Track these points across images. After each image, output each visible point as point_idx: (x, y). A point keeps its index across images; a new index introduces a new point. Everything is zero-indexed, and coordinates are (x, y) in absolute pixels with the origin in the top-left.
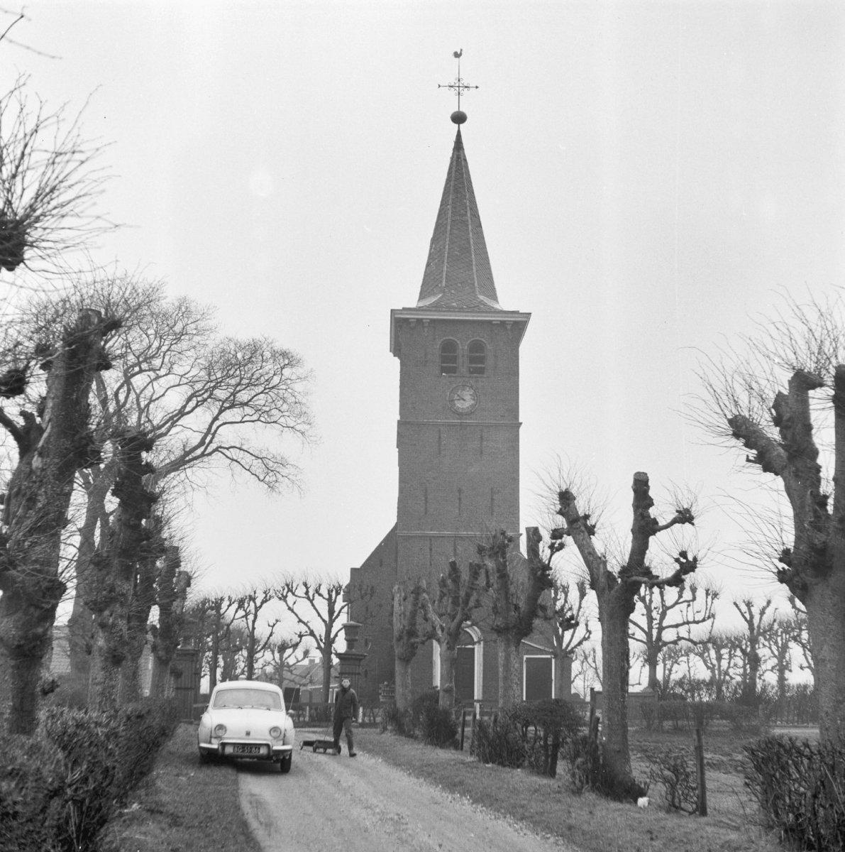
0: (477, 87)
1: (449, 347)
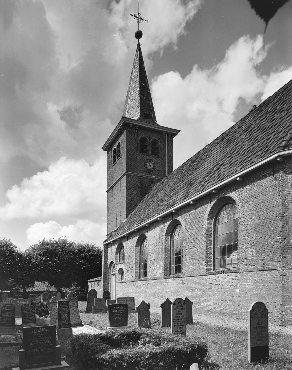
0: (131, 15)
1: (143, 140)
